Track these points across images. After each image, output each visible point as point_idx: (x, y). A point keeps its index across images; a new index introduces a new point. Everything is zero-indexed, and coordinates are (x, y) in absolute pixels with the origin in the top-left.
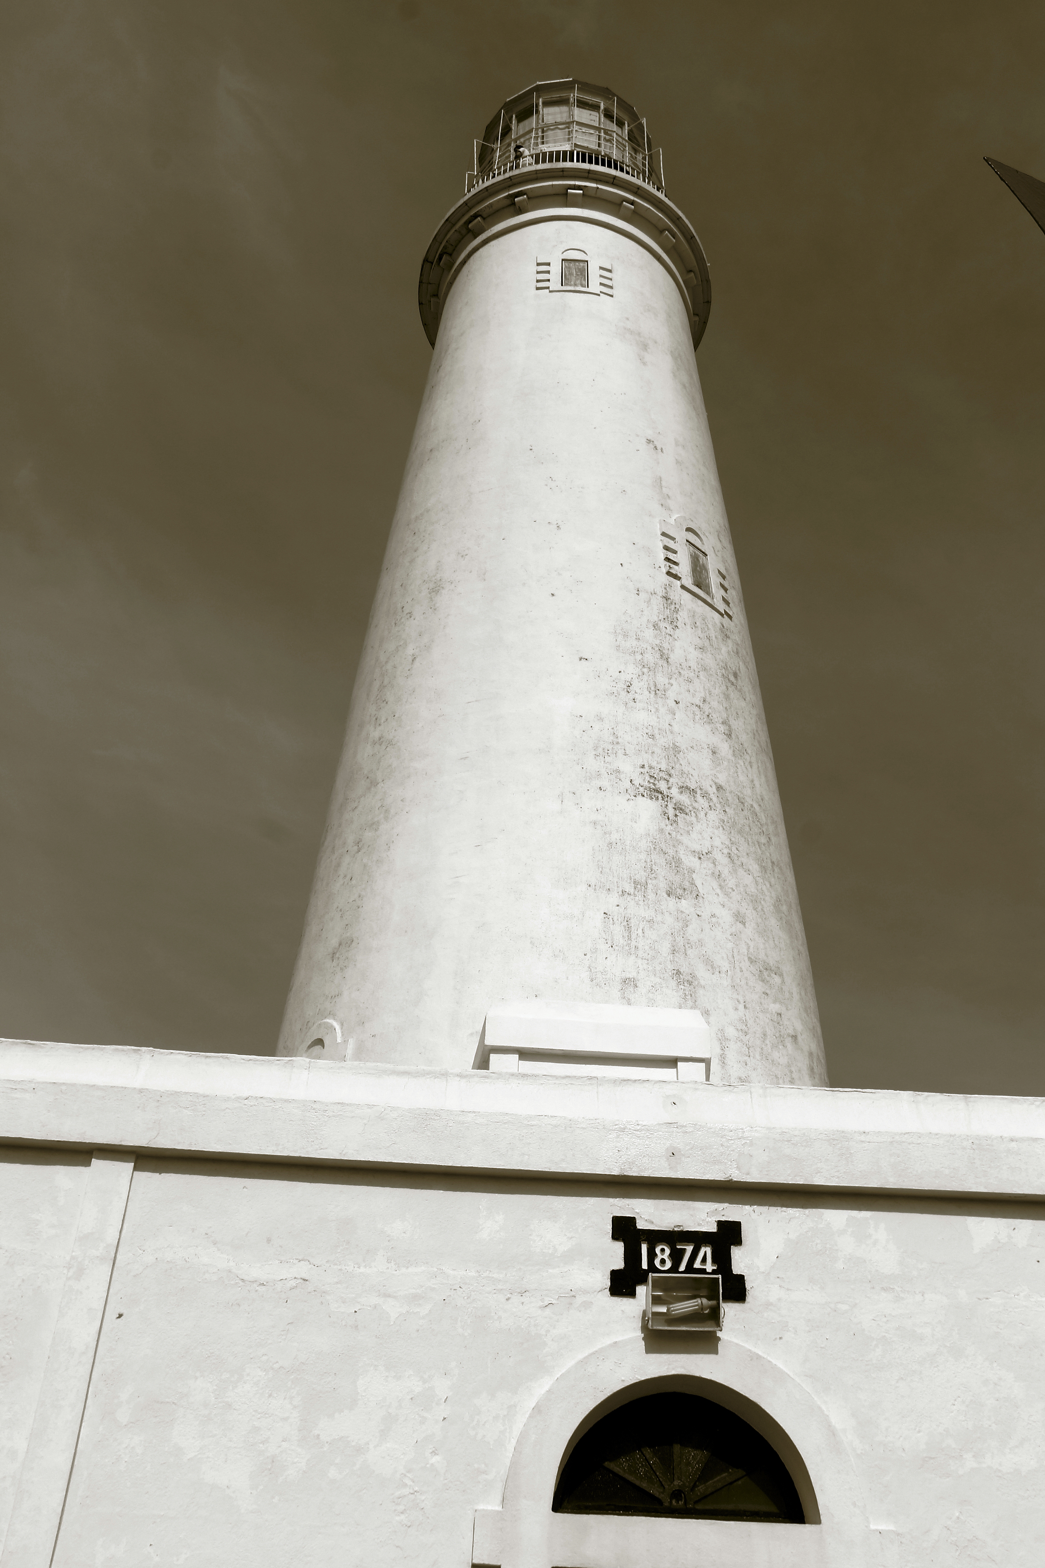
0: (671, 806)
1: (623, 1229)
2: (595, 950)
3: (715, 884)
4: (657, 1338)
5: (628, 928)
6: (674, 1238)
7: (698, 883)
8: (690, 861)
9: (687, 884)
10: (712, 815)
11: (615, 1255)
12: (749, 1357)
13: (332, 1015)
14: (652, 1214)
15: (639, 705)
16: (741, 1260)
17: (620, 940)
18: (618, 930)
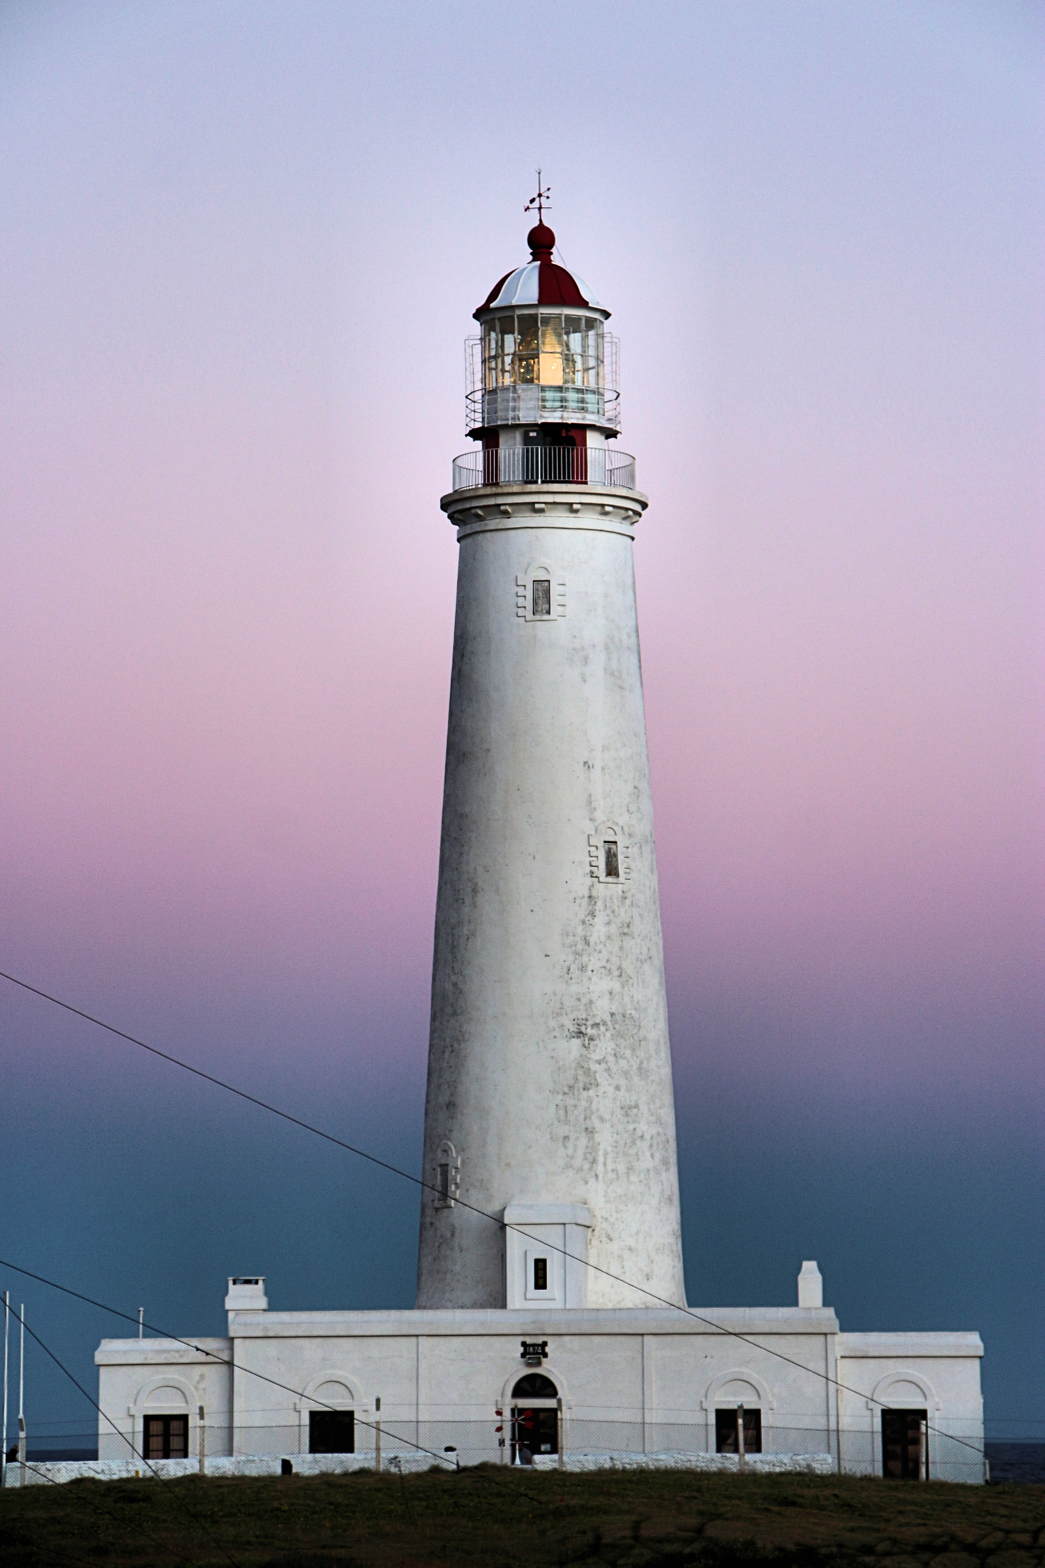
0: (587, 1039)
1: (524, 1344)
2: (552, 1124)
3: (606, 1075)
4: (529, 1365)
5: (566, 1111)
6: (534, 1345)
7: (598, 1078)
8: (594, 1067)
9: (593, 1081)
10: (608, 1034)
11: (522, 1349)
12: (548, 1368)
13: (449, 1139)
14: (529, 1340)
15: (573, 981)
16: (547, 1349)
17: (563, 1118)
18: (562, 1112)
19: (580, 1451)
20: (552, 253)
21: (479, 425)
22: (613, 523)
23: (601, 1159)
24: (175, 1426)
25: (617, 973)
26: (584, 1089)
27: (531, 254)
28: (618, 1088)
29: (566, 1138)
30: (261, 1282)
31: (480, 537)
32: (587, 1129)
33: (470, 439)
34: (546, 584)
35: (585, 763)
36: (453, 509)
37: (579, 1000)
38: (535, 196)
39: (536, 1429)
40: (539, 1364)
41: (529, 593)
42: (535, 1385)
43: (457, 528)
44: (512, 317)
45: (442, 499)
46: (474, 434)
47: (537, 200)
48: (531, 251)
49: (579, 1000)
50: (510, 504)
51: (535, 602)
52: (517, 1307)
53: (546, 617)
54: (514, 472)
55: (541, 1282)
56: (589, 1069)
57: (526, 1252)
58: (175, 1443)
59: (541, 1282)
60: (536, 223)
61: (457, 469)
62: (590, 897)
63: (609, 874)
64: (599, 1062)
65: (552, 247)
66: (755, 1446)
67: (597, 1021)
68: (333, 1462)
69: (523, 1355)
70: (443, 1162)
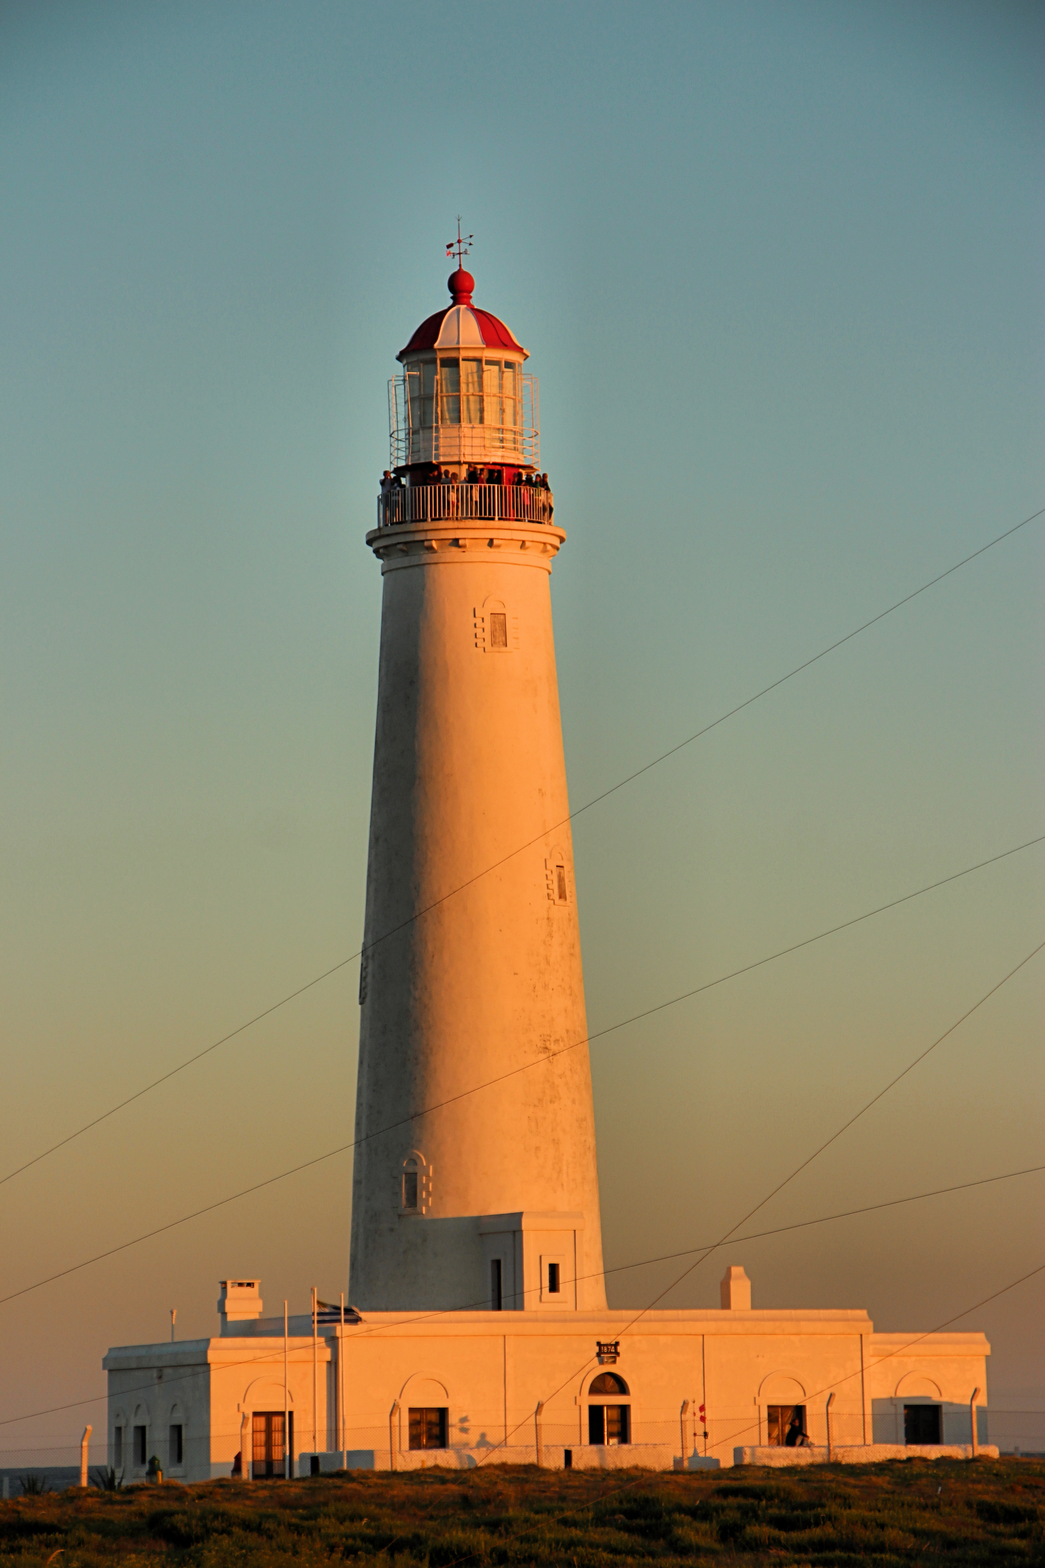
1: (599, 1344)
5: (537, 1123)
11: (597, 1349)
16: (619, 1349)
20: (471, 297)
21: (402, 463)
23: (565, 1168)
25: (568, 992)
26: (551, 1102)
27: (452, 298)
28: (574, 1102)
29: (537, 1148)
30: (256, 1286)
32: (554, 1140)
34: (502, 617)
35: (540, 790)
36: (377, 545)
37: (544, 1016)
38: (454, 241)
41: (487, 625)
43: (381, 562)
44: (436, 359)
45: (368, 534)
47: (456, 245)
48: (452, 295)
49: (544, 1016)
50: (405, 543)
51: (493, 635)
52: (534, 1309)
53: (504, 649)
54: (449, 509)
56: (553, 1083)
57: (541, 1257)
60: (456, 269)
62: (548, 919)
63: (560, 897)
64: (560, 1076)
65: (471, 291)
66: (624, 1436)
67: (558, 1037)
70: (411, 1170)
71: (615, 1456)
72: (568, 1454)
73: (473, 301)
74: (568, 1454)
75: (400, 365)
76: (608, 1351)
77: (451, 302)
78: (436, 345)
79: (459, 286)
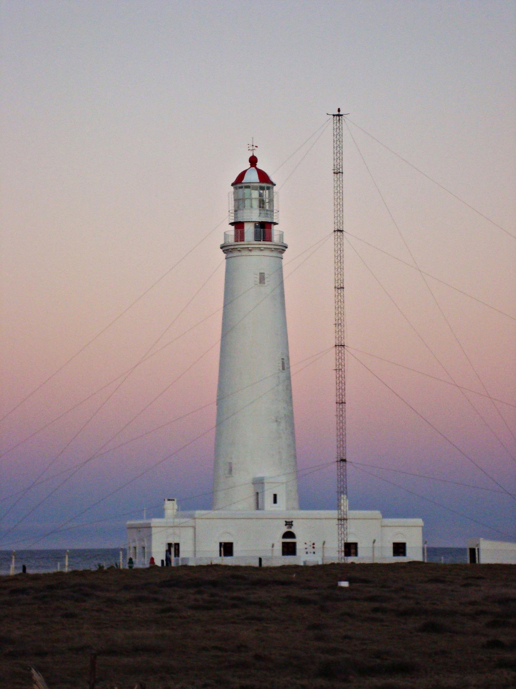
1: (286, 522)
4: (288, 528)
12: (293, 530)
14: (288, 520)
19: (302, 558)
21: (233, 221)
22: (275, 254)
24: (352, 546)
30: (176, 500)
31: (239, 258)
33: (230, 226)
36: (224, 249)
39: (289, 549)
40: (291, 528)
42: (289, 535)
43: (225, 255)
46: (232, 224)
50: (241, 248)
55: (275, 501)
58: (353, 551)
59: (275, 501)
60: (252, 155)
61: (226, 235)
68: (289, 560)
69: (286, 525)
71: (228, 561)
72: (260, 560)
73: (257, 166)
74: (260, 560)
75: (232, 187)
76: (289, 524)
77: (250, 166)
78: (243, 182)
79: (253, 161)
